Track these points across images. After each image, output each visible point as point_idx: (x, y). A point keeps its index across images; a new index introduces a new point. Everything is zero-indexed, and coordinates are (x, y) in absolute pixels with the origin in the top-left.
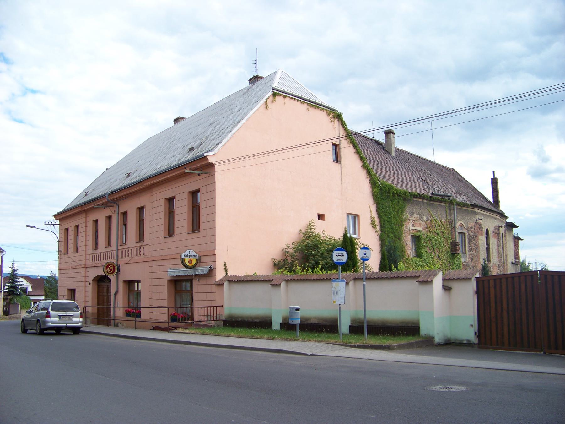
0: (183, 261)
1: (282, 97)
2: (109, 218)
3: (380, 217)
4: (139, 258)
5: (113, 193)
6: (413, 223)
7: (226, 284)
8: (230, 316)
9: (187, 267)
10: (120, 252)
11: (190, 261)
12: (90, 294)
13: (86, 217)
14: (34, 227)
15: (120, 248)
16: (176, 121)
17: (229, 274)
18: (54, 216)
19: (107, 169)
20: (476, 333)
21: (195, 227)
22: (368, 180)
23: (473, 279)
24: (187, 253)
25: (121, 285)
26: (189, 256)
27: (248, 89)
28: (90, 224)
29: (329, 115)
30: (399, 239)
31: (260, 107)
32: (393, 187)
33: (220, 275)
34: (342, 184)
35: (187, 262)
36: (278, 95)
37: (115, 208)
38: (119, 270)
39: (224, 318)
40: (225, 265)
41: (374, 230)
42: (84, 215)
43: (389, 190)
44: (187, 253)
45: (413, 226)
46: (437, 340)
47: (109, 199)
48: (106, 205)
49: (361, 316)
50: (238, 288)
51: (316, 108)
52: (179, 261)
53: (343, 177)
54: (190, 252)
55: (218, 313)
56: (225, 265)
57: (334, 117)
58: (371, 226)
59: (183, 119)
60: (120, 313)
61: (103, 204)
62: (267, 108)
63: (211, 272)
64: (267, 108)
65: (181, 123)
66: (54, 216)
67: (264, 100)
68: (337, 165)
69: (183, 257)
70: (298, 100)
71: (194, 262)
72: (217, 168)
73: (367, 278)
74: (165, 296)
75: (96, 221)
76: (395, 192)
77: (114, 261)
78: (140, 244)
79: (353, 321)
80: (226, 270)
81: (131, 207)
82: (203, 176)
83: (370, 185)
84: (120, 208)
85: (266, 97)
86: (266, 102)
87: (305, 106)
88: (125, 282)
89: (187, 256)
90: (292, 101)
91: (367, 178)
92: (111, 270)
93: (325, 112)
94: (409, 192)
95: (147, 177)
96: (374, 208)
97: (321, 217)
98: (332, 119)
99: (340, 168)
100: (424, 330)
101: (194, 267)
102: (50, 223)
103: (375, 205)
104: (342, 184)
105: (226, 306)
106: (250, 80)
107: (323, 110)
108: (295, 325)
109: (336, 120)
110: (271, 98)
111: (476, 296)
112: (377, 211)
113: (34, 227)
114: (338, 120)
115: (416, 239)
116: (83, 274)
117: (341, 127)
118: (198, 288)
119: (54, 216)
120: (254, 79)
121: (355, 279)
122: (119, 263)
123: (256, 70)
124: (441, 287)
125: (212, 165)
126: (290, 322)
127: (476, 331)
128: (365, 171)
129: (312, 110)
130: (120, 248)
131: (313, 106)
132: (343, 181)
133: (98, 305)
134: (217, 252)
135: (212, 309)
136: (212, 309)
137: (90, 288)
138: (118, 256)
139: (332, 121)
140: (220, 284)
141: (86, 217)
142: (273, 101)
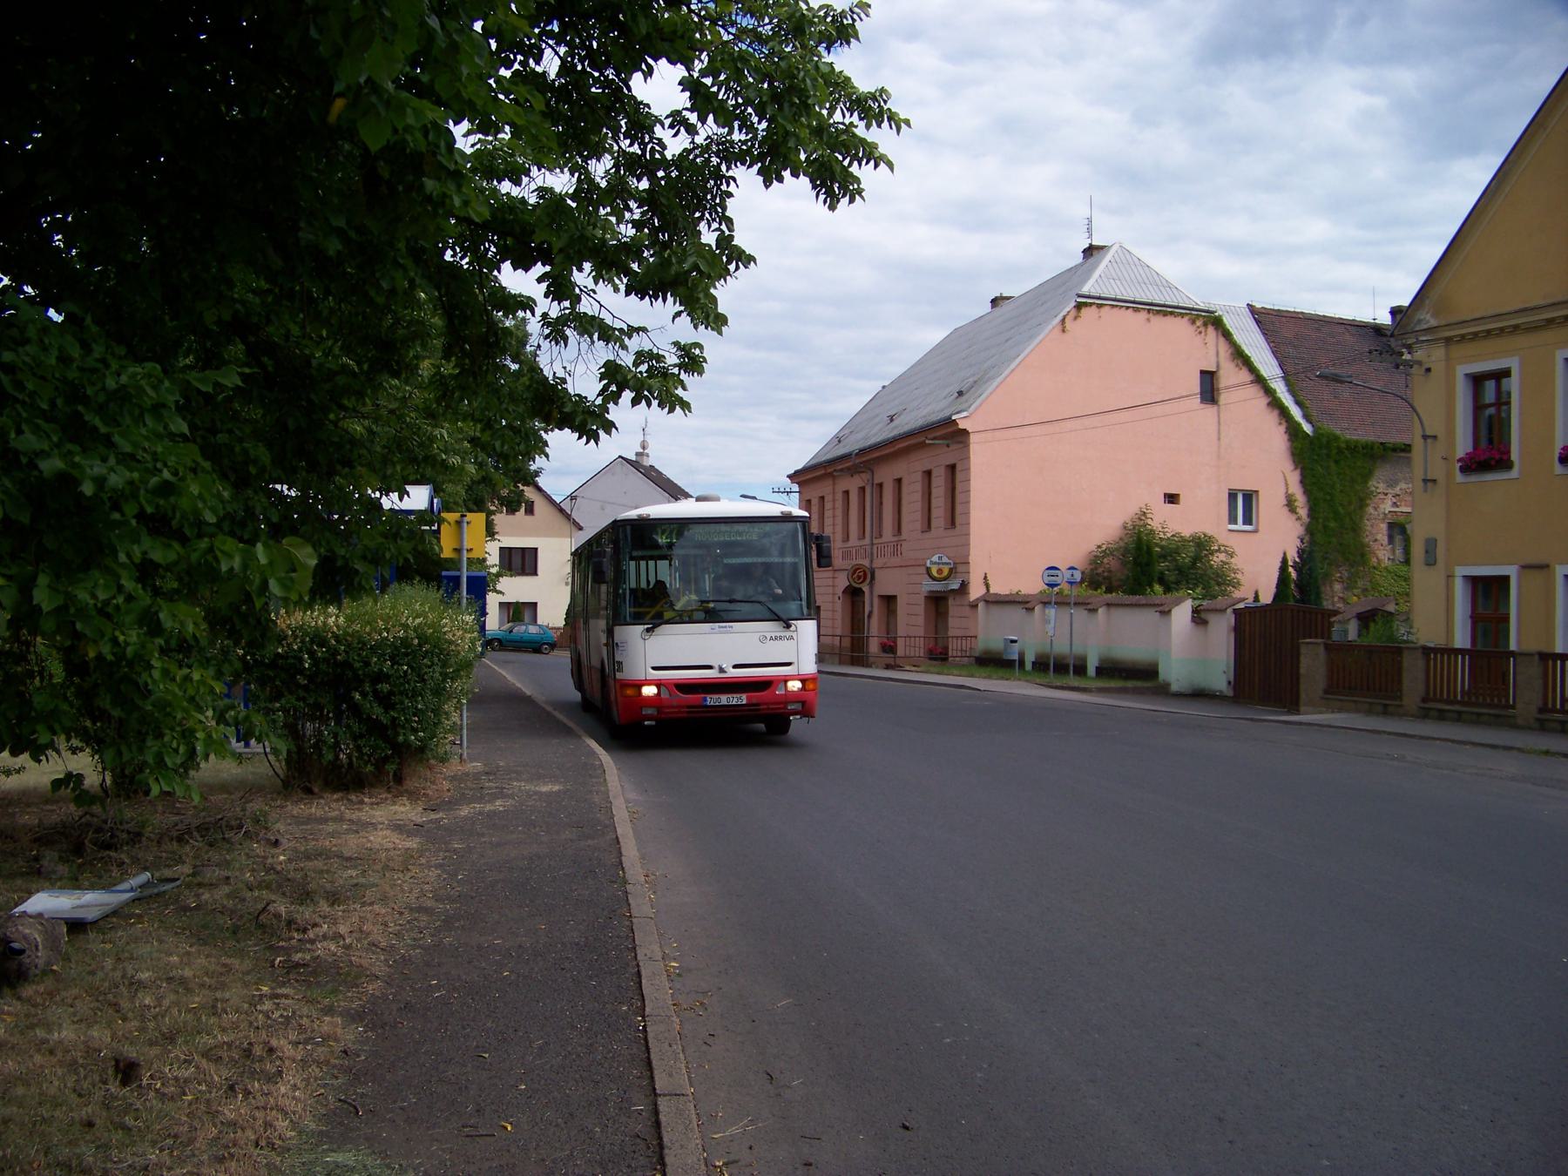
0: (928, 570)
1: (1094, 307)
2: (862, 489)
3: (1307, 492)
4: (896, 561)
5: (862, 452)
6: (1394, 500)
7: (981, 605)
8: (987, 652)
9: (934, 579)
10: (875, 547)
11: (940, 571)
12: (839, 615)
13: (834, 484)
14: (754, 498)
15: (875, 541)
16: (995, 302)
17: (992, 591)
18: (789, 476)
19: (884, 387)
20: (1229, 683)
21: (952, 523)
22: (1282, 429)
23: (1229, 611)
24: (935, 558)
25: (876, 601)
26: (939, 564)
27: (1081, 265)
28: (839, 496)
29: (1193, 322)
30: (1354, 530)
31: (1051, 331)
32: (1336, 438)
33: (976, 591)
34: (1219, 439)
35: (934, 573)
36: (1086, 304)
37: (866, 476)
38: (873, 578)
39: (977, 655)
40: (985, 578)
41: (1294, 517)
42: (829, 482)
43: (1328, 442)
44: (935, 558)
45: (1395, 504)
46: (1174, 688)
47: (857, 461)
48: (853, 471)
49: (1047, 649)
50: (996, 610)
51: (1165, 314)
52: (923, 570)
53: (1222, 428)
54: (940, 558)
55: (969, 646)
56: (985, 578)
57: (1205, 325)
58: (1286, 509)
59: (1008, 298)
60: (874, 647)
61: (848, 469)
62: (1064, 331)
63: (964, 586)
64: (1064, 331)
65: (1005, 308)
66: (789, 476)
67: (1060, 317)
68: (1210, 410)
69: (928, 565)
70: (1128, 308)
71: (946, 573)
72: (973, 438)
73: (1075, 604)
74: (921, 620)
75: (847, 493)
76: (1343, 445)
77: (866, 563)
78: (896, 539)
79: (1102, 661)
80: (987, 586)
81: (886, 474)
82: (953, 447)
83: (1286, 437)
84: (875, 477)
85: (1068, 309)
86: (1063, 320)
87: (1143, 315)
88: (881, 597)
89: (935, 563)
90: (1115, 310)
91: (1280, 424)
92: (859, 577)
93: (1186, 318)
94: (1382, 443)
95: (899, 435)
96: (1294, 478)
97: (1172, 498)
98: (1202, 329)
99: (1216, 414)
100: (1162, 676)
101: (945, 579)
102: (782, 490)
103: (1297, 473)
104: (1219, 439)
105: (981, 637)
106: (1084, 251)
107: (1182, 315)
108: (1015, 661)
109: (1211, 329)
110: (1073, 313)
111: (1232, 636)
112: (1301, 482)
113: (754, 498)
114: (1216, 329)
115: (1398, 529)
116: (830, 582)
117: (1222, 339)
118: (954, 608)
119: (789, 476)
120: (1090, 251)
121: (1109, 605)
122: (874, 566)
123: (1090, 236)
124: (1190, 617)
125: (965, 433)
126: (1005, 657)
127: (1232, 679)
128: (1276, 412)
129: (1158, 321)
130: (875, 541)
131: (1158, 312)
132: (1223, 435)
133: (852, 632)
134: (972, 559)
135: (959, 641)
136: (959, 641)
137: (839, 605)
138: (872, 554)
139: (1200, 333)
140: (974, 606)
141: (834, 484)
142: (1076, 318)
